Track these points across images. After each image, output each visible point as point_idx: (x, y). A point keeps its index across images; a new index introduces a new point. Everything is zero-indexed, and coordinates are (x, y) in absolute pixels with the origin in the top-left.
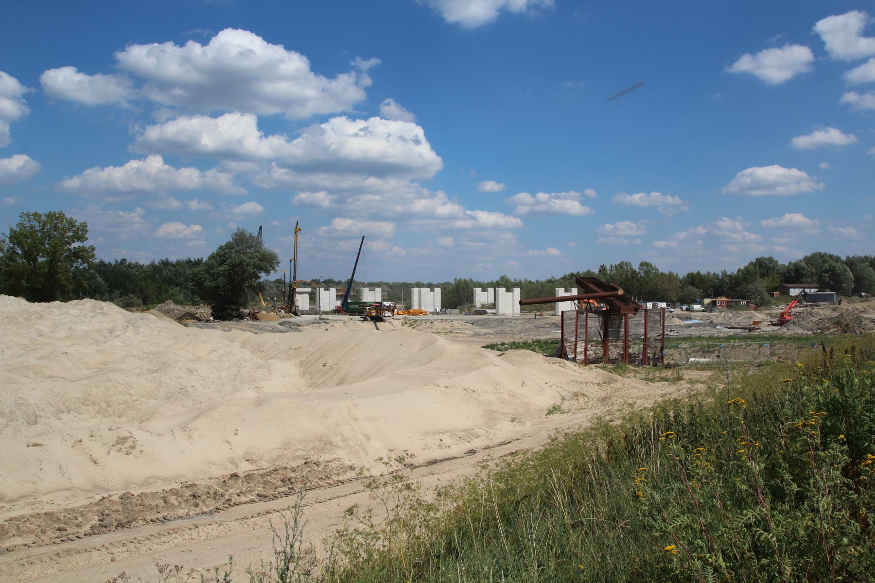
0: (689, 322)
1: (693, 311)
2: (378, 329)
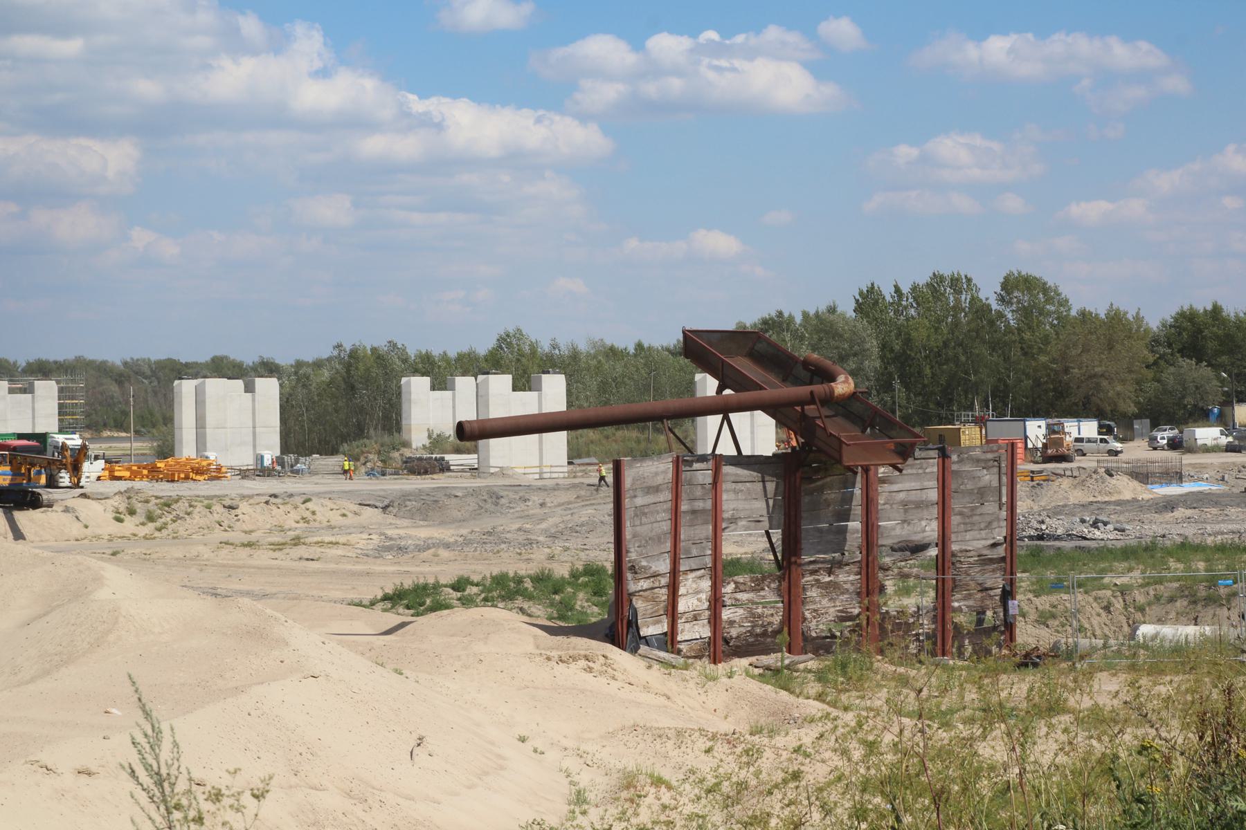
0: (1173, 490)
1: (1192, 450)
2: (18, 535)
